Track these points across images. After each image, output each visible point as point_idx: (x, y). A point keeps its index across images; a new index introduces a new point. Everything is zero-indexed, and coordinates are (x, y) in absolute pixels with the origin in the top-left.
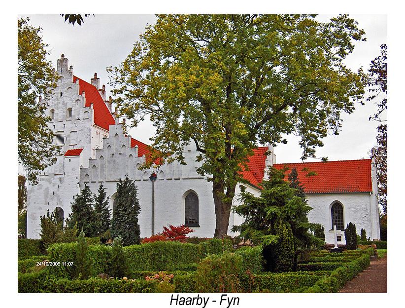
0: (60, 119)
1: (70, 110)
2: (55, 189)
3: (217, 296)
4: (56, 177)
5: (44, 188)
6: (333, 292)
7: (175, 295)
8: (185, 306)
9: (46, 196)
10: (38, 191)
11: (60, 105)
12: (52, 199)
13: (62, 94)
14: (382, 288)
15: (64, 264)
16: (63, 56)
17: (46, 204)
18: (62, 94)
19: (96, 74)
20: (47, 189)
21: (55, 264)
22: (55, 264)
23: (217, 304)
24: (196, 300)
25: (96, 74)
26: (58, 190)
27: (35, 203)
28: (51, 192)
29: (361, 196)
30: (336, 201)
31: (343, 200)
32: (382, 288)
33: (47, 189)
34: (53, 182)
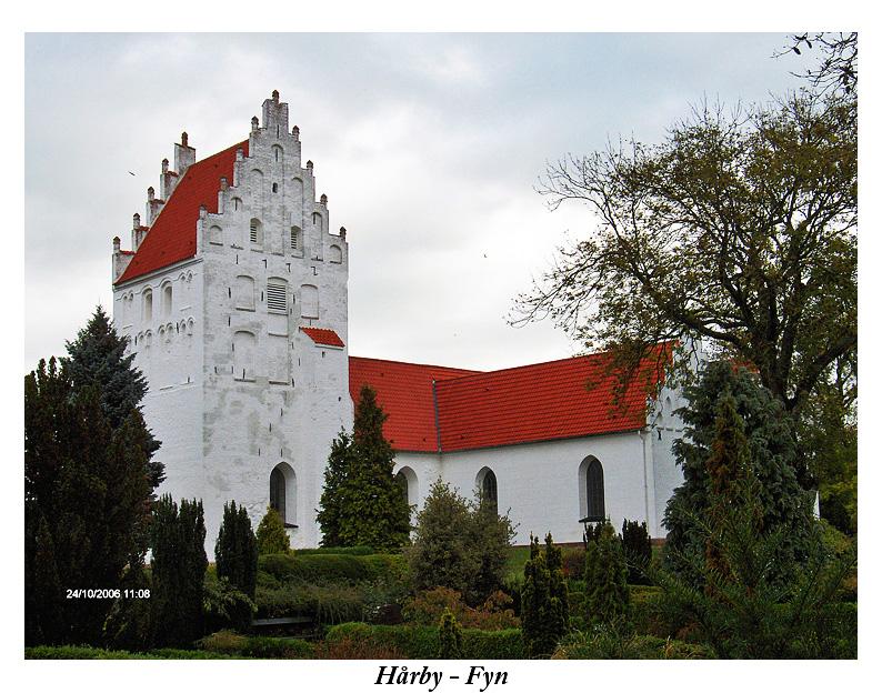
0: (276, 247)
1: (295, 231)
2: (273, 418)
3: (462, 667)
4: (274, 387)
5: (246, 412)
6: (722, 657)
7: (389, 664)
8: (395, 687)
9: (254, 432)
10: (232, 418)
11: (274, 214)
12: (268, 441)
13: (275, 186)
14: (851, 653)
15: (130, 595)
16: (276, 94)
17: (253, 452)
18: (275, 186)
19: (185, 136)
20: (254, 416)
21: (108, 594)
22: (108, 594)
23: (460, 685)
24: (418, 678)
25: (185, 136)
26: (281, 422)
27: (224, 447)
28: (264, 424)
29: (545, 447)
30: (590, 456)
31: (604, 451)
32: (851, 653)
33: (254, 416)
34: (267, 400)
